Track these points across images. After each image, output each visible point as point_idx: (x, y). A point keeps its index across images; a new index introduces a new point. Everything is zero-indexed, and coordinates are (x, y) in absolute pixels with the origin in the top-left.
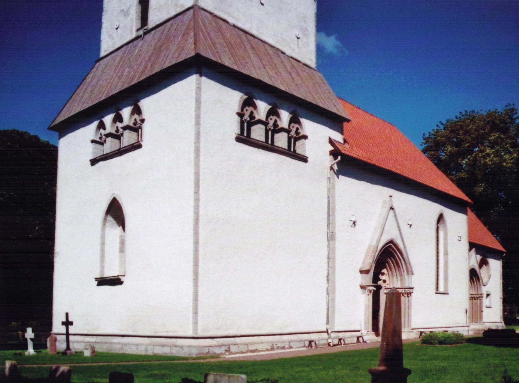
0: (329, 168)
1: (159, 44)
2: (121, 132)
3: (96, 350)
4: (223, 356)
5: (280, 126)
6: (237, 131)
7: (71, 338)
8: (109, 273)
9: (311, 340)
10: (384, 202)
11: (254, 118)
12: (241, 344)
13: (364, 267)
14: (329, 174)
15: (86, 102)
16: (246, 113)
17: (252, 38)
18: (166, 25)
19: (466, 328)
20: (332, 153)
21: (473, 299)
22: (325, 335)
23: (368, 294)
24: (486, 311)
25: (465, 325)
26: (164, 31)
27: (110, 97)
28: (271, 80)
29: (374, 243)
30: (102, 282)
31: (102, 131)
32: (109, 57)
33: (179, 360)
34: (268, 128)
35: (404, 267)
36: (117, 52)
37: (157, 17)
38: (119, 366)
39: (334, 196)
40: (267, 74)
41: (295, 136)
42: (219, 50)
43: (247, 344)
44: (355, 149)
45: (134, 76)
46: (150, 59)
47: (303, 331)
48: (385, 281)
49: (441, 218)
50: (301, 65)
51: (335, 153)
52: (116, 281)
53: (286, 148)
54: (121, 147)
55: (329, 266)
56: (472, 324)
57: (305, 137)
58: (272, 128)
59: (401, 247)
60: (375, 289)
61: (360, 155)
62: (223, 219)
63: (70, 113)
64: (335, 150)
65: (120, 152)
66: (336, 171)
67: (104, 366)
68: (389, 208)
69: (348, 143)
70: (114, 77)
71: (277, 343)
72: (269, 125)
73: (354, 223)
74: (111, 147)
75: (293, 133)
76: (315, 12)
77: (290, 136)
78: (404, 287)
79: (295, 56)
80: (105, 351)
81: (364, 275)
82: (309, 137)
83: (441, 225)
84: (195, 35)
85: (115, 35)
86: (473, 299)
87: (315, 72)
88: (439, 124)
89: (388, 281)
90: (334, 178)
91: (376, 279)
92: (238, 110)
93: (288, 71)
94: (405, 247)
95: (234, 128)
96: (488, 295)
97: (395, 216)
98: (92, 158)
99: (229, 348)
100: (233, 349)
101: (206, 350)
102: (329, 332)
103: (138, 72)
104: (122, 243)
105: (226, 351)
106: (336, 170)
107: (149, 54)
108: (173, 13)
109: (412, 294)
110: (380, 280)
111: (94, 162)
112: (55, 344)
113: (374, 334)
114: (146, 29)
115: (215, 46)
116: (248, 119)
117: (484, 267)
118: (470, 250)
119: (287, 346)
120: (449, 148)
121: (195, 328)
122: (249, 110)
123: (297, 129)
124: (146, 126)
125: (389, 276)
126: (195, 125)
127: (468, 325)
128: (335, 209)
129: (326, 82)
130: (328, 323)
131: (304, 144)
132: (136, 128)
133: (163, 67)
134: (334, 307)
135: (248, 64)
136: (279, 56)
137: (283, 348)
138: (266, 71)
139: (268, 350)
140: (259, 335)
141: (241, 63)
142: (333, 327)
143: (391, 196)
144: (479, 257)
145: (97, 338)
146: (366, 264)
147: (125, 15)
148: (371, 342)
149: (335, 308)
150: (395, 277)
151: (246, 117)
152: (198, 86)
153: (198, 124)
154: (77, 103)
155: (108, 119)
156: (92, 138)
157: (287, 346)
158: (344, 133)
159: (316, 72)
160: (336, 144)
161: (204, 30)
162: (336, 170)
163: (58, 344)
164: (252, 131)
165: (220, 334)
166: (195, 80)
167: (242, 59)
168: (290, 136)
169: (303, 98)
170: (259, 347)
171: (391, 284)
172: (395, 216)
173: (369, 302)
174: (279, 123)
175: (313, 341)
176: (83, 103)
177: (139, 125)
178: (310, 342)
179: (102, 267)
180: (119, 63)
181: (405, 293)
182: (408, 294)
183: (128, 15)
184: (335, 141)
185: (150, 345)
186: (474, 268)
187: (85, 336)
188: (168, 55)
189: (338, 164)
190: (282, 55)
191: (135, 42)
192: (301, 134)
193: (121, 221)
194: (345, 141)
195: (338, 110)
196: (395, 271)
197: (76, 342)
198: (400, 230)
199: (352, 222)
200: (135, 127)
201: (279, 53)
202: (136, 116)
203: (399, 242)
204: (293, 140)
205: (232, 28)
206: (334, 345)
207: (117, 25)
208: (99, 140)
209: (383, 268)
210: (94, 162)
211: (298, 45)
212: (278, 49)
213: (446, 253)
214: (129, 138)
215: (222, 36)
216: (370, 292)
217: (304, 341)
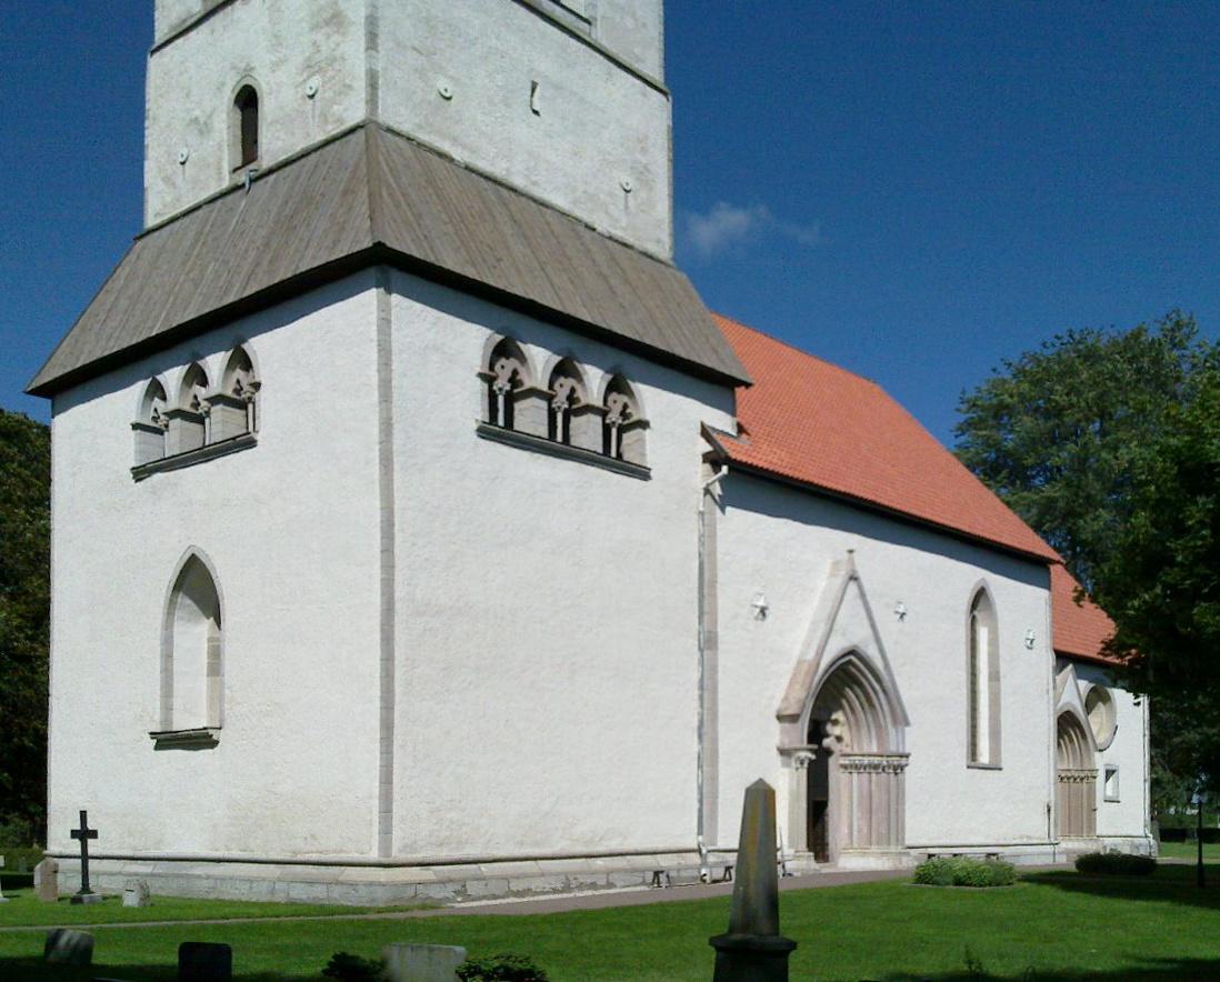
0: (702, 492)
1: (287, 210)
2: (206, 409)
3: (152, 892)
4: (449, 905)
5: (584, 402)
6: (482, 414)
7: (92, 864)
8: (183, 722)
9: (660, 869)
10: (836, 564)
11: (520, 383)
12: (492, 878)
13: (786, 709)
14: (701, 504)
15: (115, 335)
16: (500, 374)
17: (513, 195)
18: (304, 166)
19: (1049, 849)
20: (707, 458)
21: (1072, 780)
22: (695, 858)
23: (797, 769)
24: (1104, 813)
25: (1046, 841)
26: (298, 178)
27: (172, 329)
28: (560, 298)
29: (811, 655)
30: (168, 740)
31: (157, 402)
32: (168, 228)
33: (347, 913)
34: (554, 406)
35: (886, 707)
36: (187, 220)
37: (280, 143)
38: (204, 927)
39: (713, 553)
40: (548, 284)
41: (620, 421)
42: (430, 232)
43: (506, 879)
44: (765, 447)
45: (230, 283)
46: (267, 245)
47: (641, 848)
48: (839, 739)
49: (980, 597)
50: (636, 256)
51: (714, 460)
52: (200, 740)
53: (600, 450)
54: (207, 443)
55: (702, 706)
56: (1070, 840)
57: (644, 424)
58: (566, 406)
59: (878, 663)
60: (813, 757)
61: (775, 461)
62: (451, 608)
63: (78, 359)
64: (715, 451)
66: (717, 498)
67: (168, 927)
68: (847, 577)
69: (748, 434)
70: (182, 279)
71: (578, 876)
72: (555, 400)
73: (763, 611)
74: (181, 441)
75: (614, 417)
76: (668, 126)
77: (608, 421)
78: (885, 753)
79: (618, 233)
80: (176, 894)
81: (787, 725)
82: (652, 425)
83: (982, 613)
85: (179, 180)
86: (1072, 780)
87: (668, 271)
88: (1002, 368)
89: (847, 738)
90: (713, 513)
91: (816, 733)
92: (482, 367)
93: (600, 274)
94: (887, 665)
95: (471, 405)
96: (1109, 773)
97: (863, 595)
98: (134, 464)
99: (464, 886)
100: (472, 889)
101: (410, 892)
102: (704, 851)
103: (239, 273)
104: (216, 654)
105: (457, 893)
106: (719, 496)
107: (263, 232)
108: (320, 137)
109: (906, 769)
110: (827, 736)
111: (140, 473)
112: (56, 877)
113: (813, 858)
114: (256, 170)
115: (421, 222)
116: (508, 387)
117: (1101, 708)
118: (1059, 668)
119: (602, 882)
120: (1028, 421)
121: (386, 842)
122: (506, 367)
123: (625, 406)
124: (262, 397)
125: (850, 728)
126: (380, 403)
127: (1053, 841)
128: (716, 582)
129: (695, 294)
130: (700, 832)
131: (642, 441)
132: (241, 402)
133: (298, 267)
134: (715, 796)
135: (502, 263)
136: (579, 237)
137: (593, 886)
138: (547, 276)
139: (555, 891)
140: (535, 859)
141: (484, 261)
142: (713, 840)
143: (851, 552)
144: (1084, 685)
145: (155, 865)
146: (792, 701)
147: (201, 133)
148: (803, 874)
149: (717, 797)
150: (864, 731)
151: (502, 383)
152: (383, 315)
153: (386, 401)
154: (93, 336)
155: (172, 377)
156: (134, 420)
157: (602, 882)
158: (738, 413)
159: (672, 270)
160: (714, 435)
162: (719, 496)
163: (60, 878)
164: (516, 413)
165: (444, 854)
166: (374, 308)
167: (486, 249)
168: (608, 421)
169: (637, 338)
170: (536, 884)
171: (855, 746)
172: (863, 595)
173: (798, 785)
174: (579, 393)
175: (662, 872)
176: (109, 339)
177: (248, 394)
178: (657, 874)
179: (167, 708)
180: (193, 246)
181: (889, 767)
182: (895, 768)
183: (209, 132)
184: (713, 429)
185: (279, 880)
186: (1071, 709)
187: (129, 862)
188: (310, 239)
189: (722, 481)
190: (588, 234)
191: (230, 198)
192: (635, 418)
193: (210, 604)
194: (741, 429)
195: (723, 362)
196: (864, 720)
197: (104, 874)
198: (873, 626)
199: (758, 610)
200: (237, 397)
201: (581, 229)
202: (239, 373)
203: (871, 652)
204: (614, 432)
206: (715, 881)
207: (182, 156)
208: (153, 424)
209: (836, 710)
210: (140, 473)
211: (626, 207)
212: (579, 221)
213: (995, 677)
214: (222, 424)
215: (438, 196)
216: (802, 763)
217: (643, 871)
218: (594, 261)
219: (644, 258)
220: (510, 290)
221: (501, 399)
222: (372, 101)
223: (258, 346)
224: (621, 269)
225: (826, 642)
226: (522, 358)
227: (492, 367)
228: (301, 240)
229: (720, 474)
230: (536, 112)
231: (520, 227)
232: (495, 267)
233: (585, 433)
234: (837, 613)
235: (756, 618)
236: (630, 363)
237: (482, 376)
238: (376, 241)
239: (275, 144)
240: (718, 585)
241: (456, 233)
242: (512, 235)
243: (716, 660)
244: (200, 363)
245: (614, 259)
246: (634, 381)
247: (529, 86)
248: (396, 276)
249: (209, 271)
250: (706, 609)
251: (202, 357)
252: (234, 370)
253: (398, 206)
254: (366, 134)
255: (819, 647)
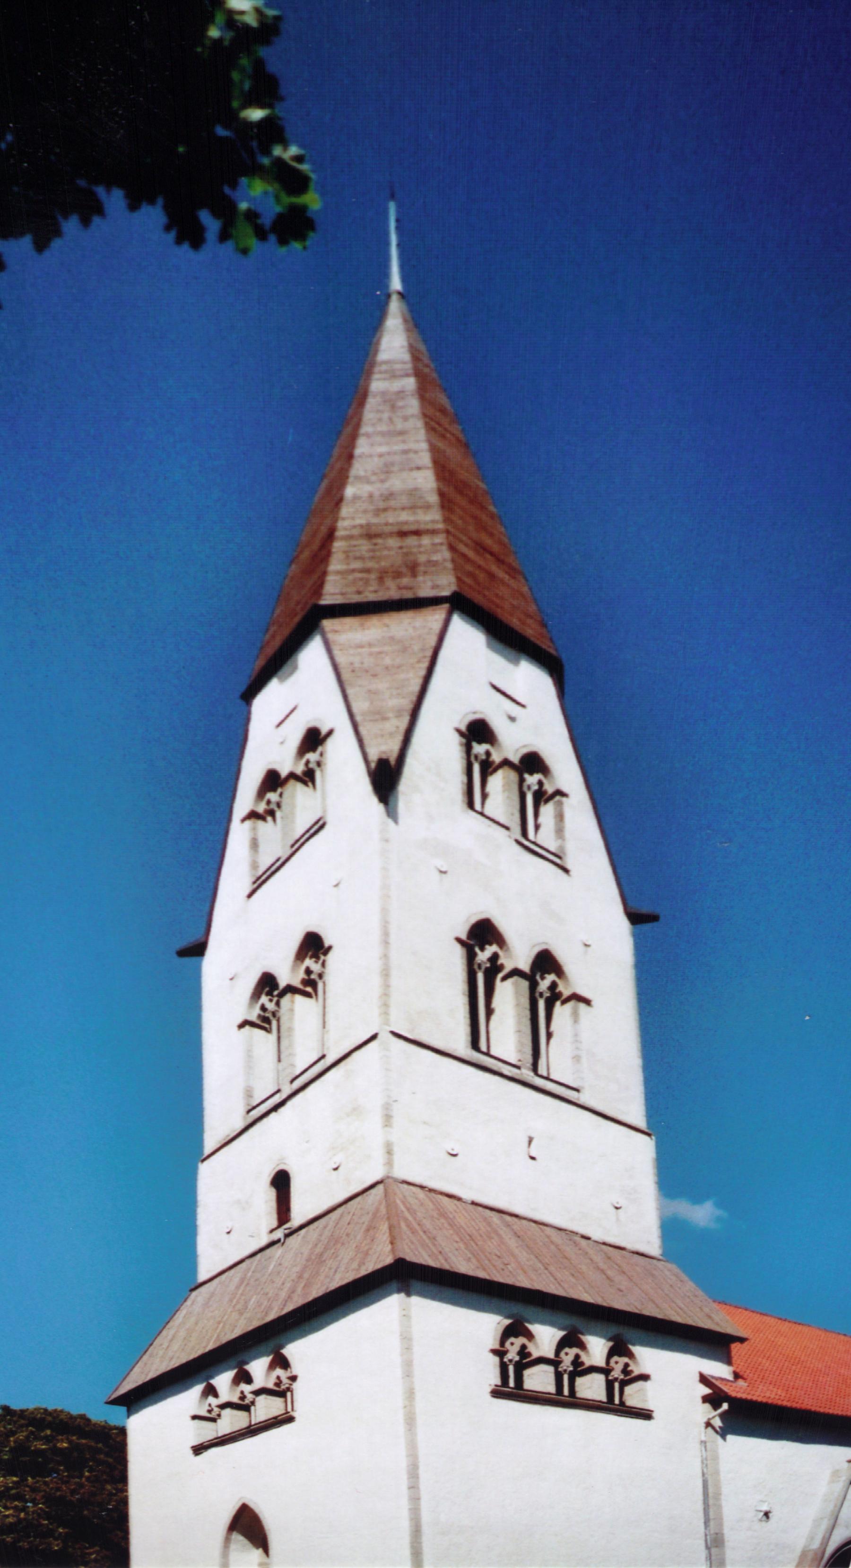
0: (704, 1425)
14: (703, 1435)
20: (706, 1399)
36: (232, 1271)
46: (300, 1277)
51: (714, 1399)
54: (253, 1423)
57: (645, 1377)
58: (571, 1369)
64: (714, 1393)
65: (252, 1431)
73: (767, 1514)
75: (617, 1373)
84: (391, 1228)
87: (660, 1264)
93: (598, 1268)
106: (720, 1427)
111: (198, 1450)
114: (289, 1228)
115: (436, 1243)
116: (517, 1358)
122: (514, 1346)
129: (685, 1277)
132: (280, 1392)
136: (576, 1244)
151: (512, 1355)
152: (404, 1313)
153: (408, 1376)
155: (223, 1381)
158: (734, 1360)
159: (662, 1263)
161: (410, 1218)
167: (494, 1257)
177: (287, 1386)
180: (238, 1288)
184: (713, 1377)
189: (723, 1416)
190: (584, 1242)
194: (737, 1376)
195: (718, 1324)
199: (762, 1514)
202: (279, 1372)
204: (617, 1385)
205: (471, 1207)
208: (208, 1415)
218: (591, 1260)
219: (636, 1256)
220: (518, 1284)
221: (511, 1369)
222: (389, 1163)
223: (293, 1350)
224: (617, 1264)
225: (831, 1535)
226: (530, 1336)
227: (502, 1343)
228: (330, 1269)
229: (720, 1411)
230: (533, 1158)
231: (523, 1241)
232: (503, 1270)
233: (590, 1388)
234: (839, 1512)
235: (761, 1520)
236: (628, 1333)
237: (494, 1352)
238: (397, 1257)
239: (300, 1211)
240: (723, 1497)
241: (466, 1248)
242: (517, 1247)
243: (724, 1554)
244: (247, 1367)
245: (609, 1258)
246: (634, 1345)
247: (526, 1140)
248: (416, 1285)
249: (252, 1302)
250: (712, 1515)
251: (247, 1363)
252: (275, 1368)
253: (414, 1232)
254: (384, 1186)
255: (824, 1538)
